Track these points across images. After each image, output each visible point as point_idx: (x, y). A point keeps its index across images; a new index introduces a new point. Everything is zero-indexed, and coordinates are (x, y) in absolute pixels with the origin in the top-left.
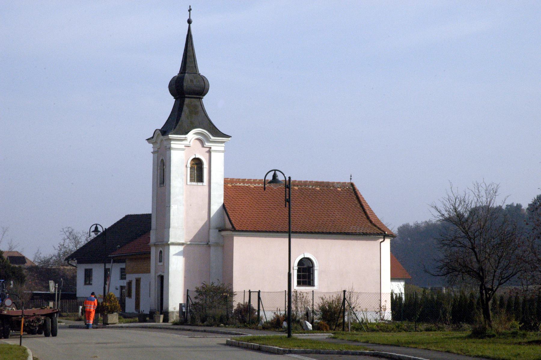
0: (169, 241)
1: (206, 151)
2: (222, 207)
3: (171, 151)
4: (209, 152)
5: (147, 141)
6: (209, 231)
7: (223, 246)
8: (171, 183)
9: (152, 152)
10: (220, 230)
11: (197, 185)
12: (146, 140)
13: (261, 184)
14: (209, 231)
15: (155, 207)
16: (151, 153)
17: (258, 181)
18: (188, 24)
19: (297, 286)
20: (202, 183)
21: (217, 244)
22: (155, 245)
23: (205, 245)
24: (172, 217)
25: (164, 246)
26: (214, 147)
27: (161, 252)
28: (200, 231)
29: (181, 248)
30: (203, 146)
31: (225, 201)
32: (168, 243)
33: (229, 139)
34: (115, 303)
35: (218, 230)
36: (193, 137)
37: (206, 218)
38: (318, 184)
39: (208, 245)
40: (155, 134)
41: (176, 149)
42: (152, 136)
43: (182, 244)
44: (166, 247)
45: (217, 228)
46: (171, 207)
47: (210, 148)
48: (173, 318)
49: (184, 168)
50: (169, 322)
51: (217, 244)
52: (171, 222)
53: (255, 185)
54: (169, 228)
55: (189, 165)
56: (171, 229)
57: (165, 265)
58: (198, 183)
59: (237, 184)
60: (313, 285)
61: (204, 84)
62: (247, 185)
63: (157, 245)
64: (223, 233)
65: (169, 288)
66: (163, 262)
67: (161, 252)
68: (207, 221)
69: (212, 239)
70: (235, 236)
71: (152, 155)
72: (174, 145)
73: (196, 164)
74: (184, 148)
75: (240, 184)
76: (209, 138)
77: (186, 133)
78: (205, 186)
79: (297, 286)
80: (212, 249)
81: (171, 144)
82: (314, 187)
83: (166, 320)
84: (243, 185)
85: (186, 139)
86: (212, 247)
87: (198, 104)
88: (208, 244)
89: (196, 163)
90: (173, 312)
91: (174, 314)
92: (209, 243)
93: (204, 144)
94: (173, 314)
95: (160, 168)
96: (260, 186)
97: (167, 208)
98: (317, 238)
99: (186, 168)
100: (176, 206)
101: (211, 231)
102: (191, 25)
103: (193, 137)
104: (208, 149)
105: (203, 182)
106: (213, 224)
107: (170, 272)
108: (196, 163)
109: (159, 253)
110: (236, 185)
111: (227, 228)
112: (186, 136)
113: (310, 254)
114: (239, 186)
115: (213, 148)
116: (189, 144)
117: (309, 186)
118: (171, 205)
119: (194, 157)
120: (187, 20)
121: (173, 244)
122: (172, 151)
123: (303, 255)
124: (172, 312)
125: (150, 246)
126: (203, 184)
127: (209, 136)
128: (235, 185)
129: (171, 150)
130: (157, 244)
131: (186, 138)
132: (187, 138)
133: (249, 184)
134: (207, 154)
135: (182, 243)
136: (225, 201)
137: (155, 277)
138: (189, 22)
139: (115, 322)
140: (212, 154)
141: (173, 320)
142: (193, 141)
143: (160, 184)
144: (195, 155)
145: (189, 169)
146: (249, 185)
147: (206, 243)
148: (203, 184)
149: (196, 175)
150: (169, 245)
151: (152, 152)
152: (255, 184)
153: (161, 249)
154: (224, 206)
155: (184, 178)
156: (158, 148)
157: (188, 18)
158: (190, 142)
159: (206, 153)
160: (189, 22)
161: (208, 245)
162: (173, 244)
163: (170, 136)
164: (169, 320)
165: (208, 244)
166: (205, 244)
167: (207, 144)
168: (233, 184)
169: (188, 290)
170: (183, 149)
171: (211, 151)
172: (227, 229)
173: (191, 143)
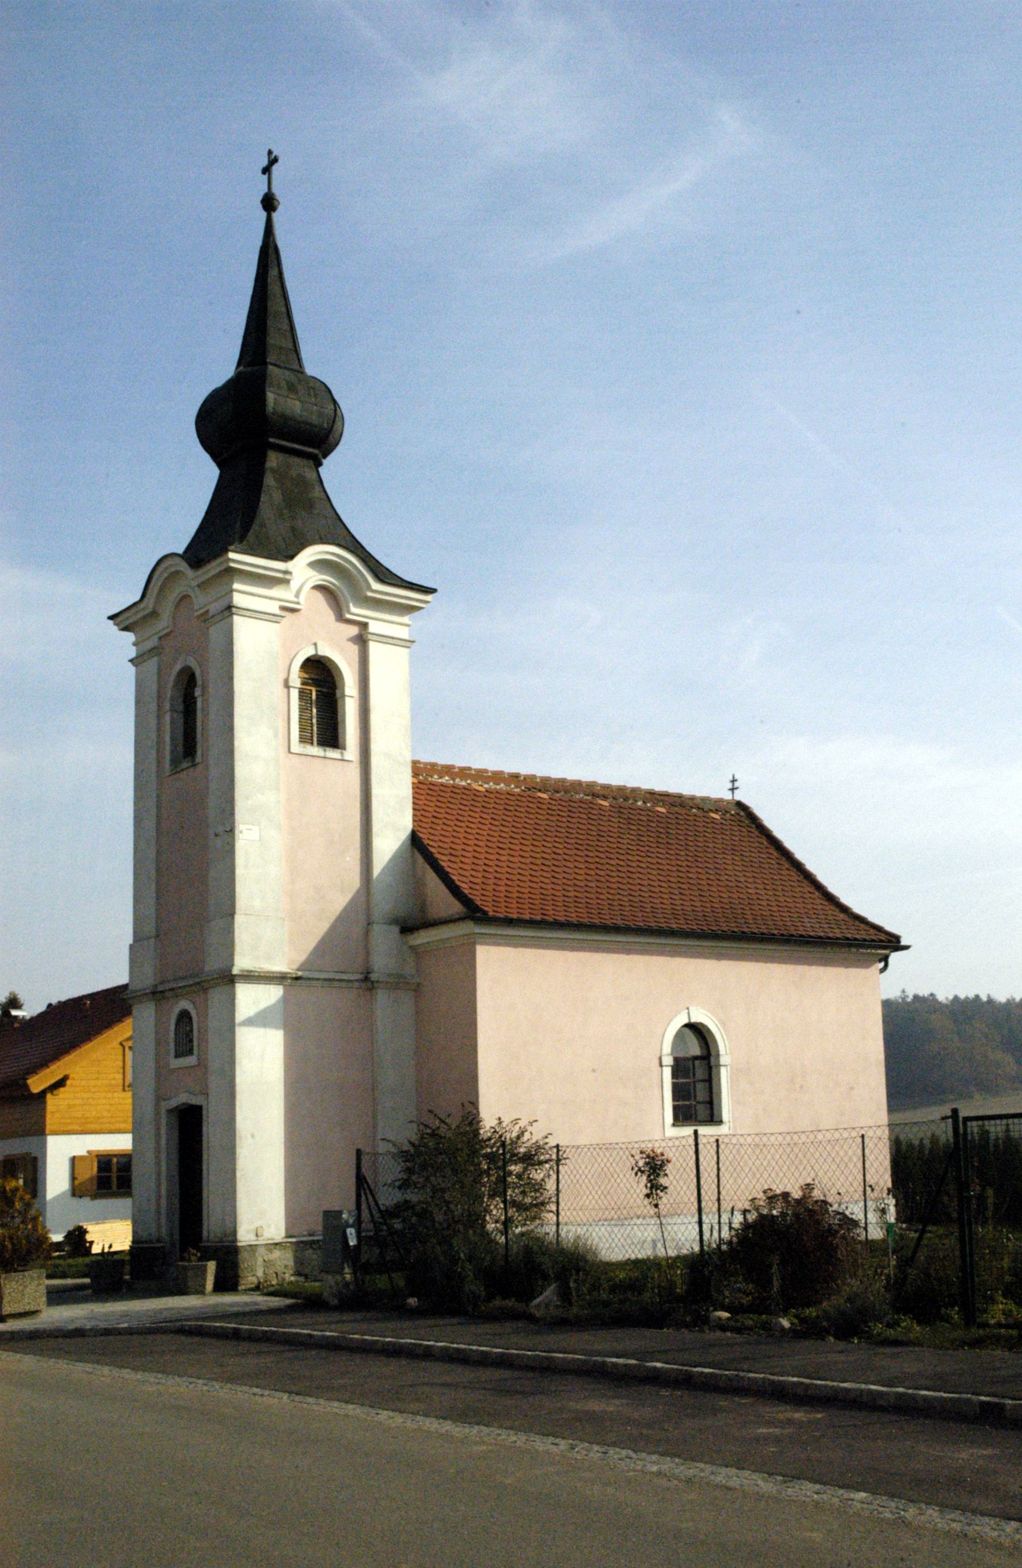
0: (233, 965)
1: (348, 637)
2: (409, 842)
3: (235, 618)
4: (362, 640)
5: (111, 622)
6: (367, 933)
7: (417, 989)
8: (236, 743)
9: (131, 661)
10: (407, 927)
11: (325, 758)
12: (111, 618)
13: (502, 785)
14: (367, 933)
15: (152, 853)
16: (130, 664)
17: (490, 774)
18: (264, 214)
19: (674, 1125)
20: (339, 751)
21: (398, 982)
22: (154, 993)
23: (357, 984)
24: (240, 872)
25: (205, 990)
26: (379, 624)
27: (184, 1017)
28: (333, 928)
29: (273, 994)
30: (340, 618)
31: (416, 824)
32: (231, 971)
33: (429, 598)
34: (30, 1226)
35: (396, 929)
36: (311, 577)
37: (354, 881)
38: (653, 796)
39: (367, 981)
40: (154, 580)
41: (248, 613)
42: (137, 598)
43: (279, 978)
44: (216, 996)
45: (395, 921)
46: (237, 832)
47: (365, 625)
48: (253, 1270)
49: (279, 690)
50: (240, 1288)
51: (398, 982)
52: (237, 890)
53: (486, 786)
54: (232, 914)
55: (296, 681)
56: (239, 919)
57: (214, 1065)
58: (328, 749)
59: (432, 777)
60: (720, 1122)
61: (332, 413)
62: (463, 783)
63: (161, 992)
64: (422, 938)
65: (238, 1150)
66: (195, 1052)
67: (184, 1017)
68: (358, 891)
69: (382, 962)
70: (482, 944)
71: (132, 670)
72: (243, 595)
73: (316, 682)
74: (278, 612)
75: (440, 778)
76: (363, 584)
77: (291, 557)
78: (351, 764)
79: (674, 1125)
80: (382, 997)
81: (235, 594)
82: (649, 805)
83: (227, 1282)
84: (451, 782)
85: (288, 577)
86: (379, 991)
87: (311, 475)
88: (366, 979)
89: (313, 676)
90: (253, 1248)
91: (257, 1254)
92: (374, 977)
93: (344, 609)
94: (254, 1255)
95: (172, 705)
96: (501, 789)
97: (219, 843)
98: (719, 957)
99: (286, 690)
100: (256, 828)
101: (376, 929)
102: (275, 215)
103: (311, 577)
104: (354, 630)
105: (344, 749)
106: (384, 904)
107: (238, 1088)
108: (312, 679)
109: (173, 1022)
110: (430, 779)
111: (436, 917)
112: (289, 565)
113: (704, 1012)
114: (442, 785)
115: (374, 627)
116: (296, 600)
117: (636, 801)
118: (236, 824)
119: (310, 652)
120: (260, 198)
121: (251, 977)
122: (237, 620)
123: (686, 1016)
124: (251, 1246)
125: (130, 1001)
126: (342, 754)
127: (363, 575)
128: (426, 779)
129: (232, 614)
130: (160, 988)
131: (286, 572)
132: (290, 573)
133: (469, 782)
134: (354, 649)
135: (280, 973)
136: (416, 824)
137: (157, 1113)
138: (269, 203)
139: (33, 1309)
140: (373, 647)
141: (256, 1282)
142: (308, 592)
143: (175, 762)
144: (315, 644)
145: (295, 694)
146: (469, 784)
147: (361, 976)
148: (342, 754)
149: (314, 721)
150: (229, 979)
151: (131, 661)
152: (488, 783)
153: (184, 1004)
154: (415, 840)
155: (281, 725)
156: (161, 634)
157: (266, 190)
158: (297, 595)
159: (350, 644)
160: (269, 203)
161: (367, 981)
162: (251, 977)
163: (232, 555)
164: (242, 1282)
165: (366, 979)
166: (357, 980)
167: (356, 611)
168: (421, 777)
169: (359, 1153)
170: (272, 618)
171: (370, 637)
172: (435, 920)
173: (302, 599)
